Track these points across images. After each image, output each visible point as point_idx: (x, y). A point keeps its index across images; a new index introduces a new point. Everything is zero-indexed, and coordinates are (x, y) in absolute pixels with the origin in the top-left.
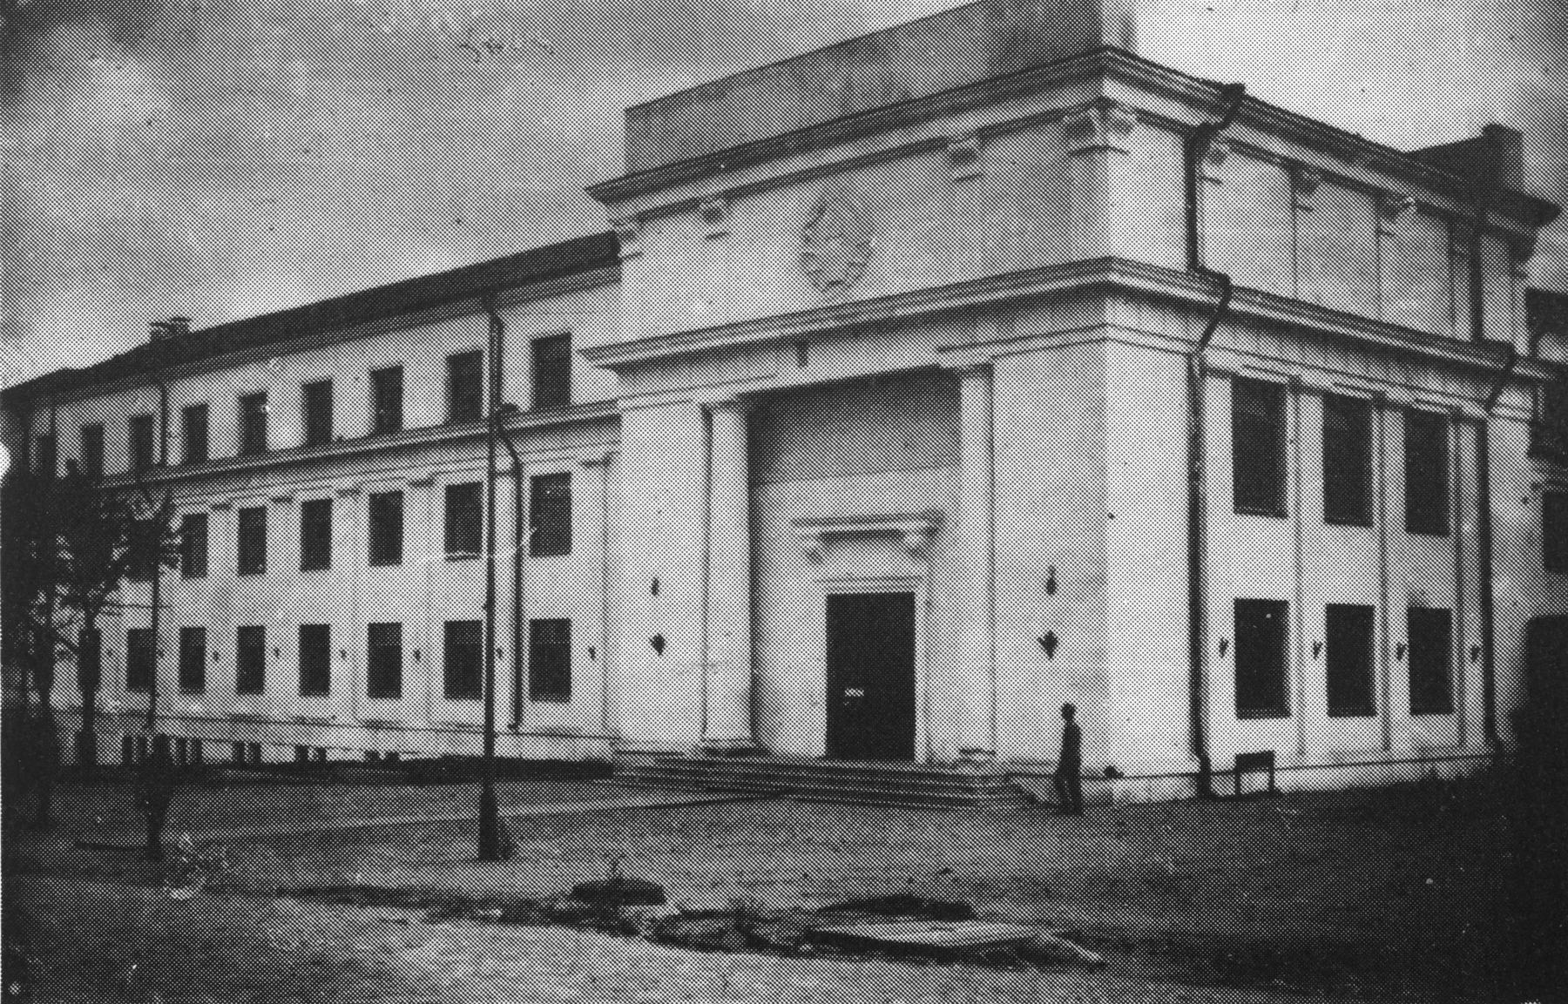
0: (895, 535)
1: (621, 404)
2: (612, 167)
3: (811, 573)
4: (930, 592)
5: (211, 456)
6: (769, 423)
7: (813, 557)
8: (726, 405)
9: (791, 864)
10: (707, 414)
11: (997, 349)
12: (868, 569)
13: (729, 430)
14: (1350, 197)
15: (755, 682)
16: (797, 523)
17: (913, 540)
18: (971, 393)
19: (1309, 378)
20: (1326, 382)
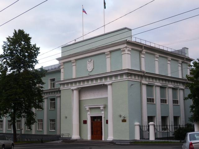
0: (99, 108)
2: (60, 56)
6: (81, 91)
8: (75, 89)
12: (96, 114)
13: (76, 93)
18: (109, 87)
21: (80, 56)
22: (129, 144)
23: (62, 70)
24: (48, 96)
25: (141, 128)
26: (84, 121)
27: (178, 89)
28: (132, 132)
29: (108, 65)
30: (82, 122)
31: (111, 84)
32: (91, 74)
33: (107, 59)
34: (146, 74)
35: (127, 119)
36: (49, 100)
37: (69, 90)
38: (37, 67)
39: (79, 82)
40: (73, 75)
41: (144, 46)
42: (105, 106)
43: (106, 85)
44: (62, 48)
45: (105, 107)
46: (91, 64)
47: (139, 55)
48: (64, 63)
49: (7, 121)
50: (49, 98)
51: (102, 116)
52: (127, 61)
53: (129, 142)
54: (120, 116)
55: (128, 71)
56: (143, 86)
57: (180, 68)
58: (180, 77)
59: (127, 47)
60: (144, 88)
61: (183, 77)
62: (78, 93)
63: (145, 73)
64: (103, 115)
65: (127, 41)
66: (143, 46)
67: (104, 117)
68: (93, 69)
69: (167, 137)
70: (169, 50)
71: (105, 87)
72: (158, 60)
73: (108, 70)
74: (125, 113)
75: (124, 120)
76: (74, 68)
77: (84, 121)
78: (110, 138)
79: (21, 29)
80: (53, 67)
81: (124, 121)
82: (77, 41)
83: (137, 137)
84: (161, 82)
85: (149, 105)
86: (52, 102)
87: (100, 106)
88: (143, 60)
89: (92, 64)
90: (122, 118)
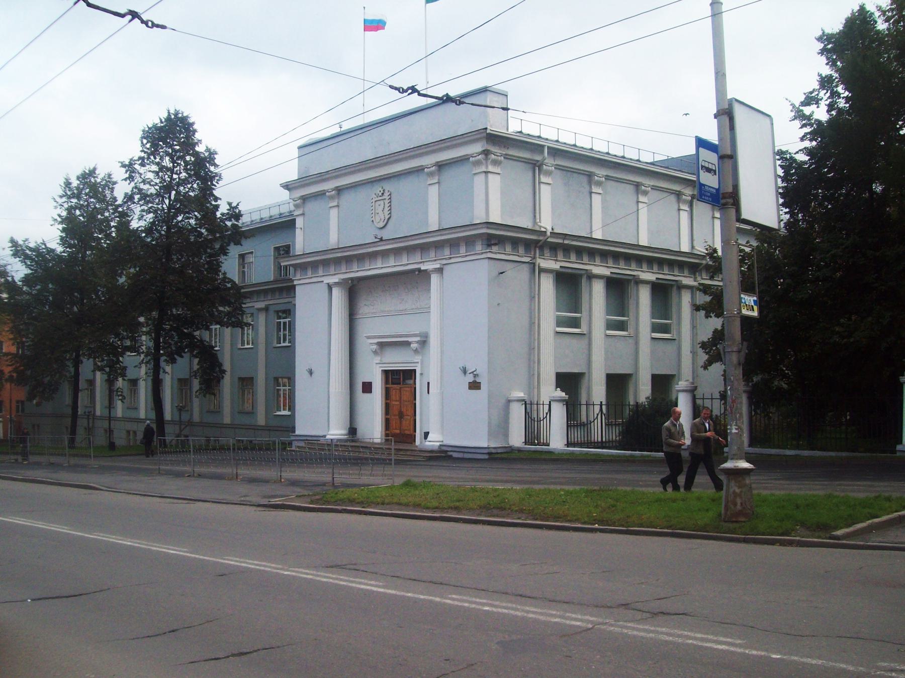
0: (408, 344)
1: (295, 283)
2: (292, 175)
3: (377, 359)
4: (422, 367)
5: (717, 143)
6: (354, 291)
7: (375, 352)
8: (336, 284)
9: (379, 479)
10: (330, 287)
11: (445, 262)
12: (397, 360)
13: (339, 297)
14: (582, 176)
15: (233, 655)
16: (368, 338)
17: (414, 346)
18: (434, 278)
19: (597, 270)
20: (606, 272)
21: (346, 178)
22: (486, 457)
23: (299, 222)
24: (271, 302)
25: (528, 410)
26: (364, 383)
27: (675, 288)
28: (503, 427)
29: (429, 208)
30: (359, 387)
31: (440, 271)
32: (386, 235)
33: (430, 188)
34: (550, 237)
35: (483, 381)
36: (272, 314)
37: (319, 284)
38: (29, 271)
39: (348, 260)
40: (331, 233)
41: (548, 147)
42: (423, 339)
43: (426, 271)
44: (300, 148)
45: (424, 342)
46: (382, 202)
47: (530, 174)
48: (305, 199)
49: (176, 382)
50: (272, 309)
51: (415, 370)
52: (495, 198)
53: (486, 451)
54: (465, 371)
55: (488, 228)
56: (543, 275)
57: (684, 216)
58: (685, 248)
59: (488, 151)
60: (547, 286)
61: (693, 247)
62: (347, 294)
63: (549, 234)
64: (419, 365)
65: (488, 131)
66: (543, 146)
67: (421, 374)
68: (389, 219)
69: (600, 439)
70: (647, 158)
71: (419, 278)
72: (601, 192)
73: (333, 239)
74: (479, 364)
75: (475, 382)
76: (434, 191)
77: (364, 383)
78: (435, 440)
79: (140, 134)
80: (265, 215)
81: (475, 385)
82: (346, 126)
83: (517, 439)
84: (610, 264)
85: (567, 340)
86: (282, 321)
87: (410, 339)
88: (545, 193)
89: (387, 202)
90: (470, 378)
